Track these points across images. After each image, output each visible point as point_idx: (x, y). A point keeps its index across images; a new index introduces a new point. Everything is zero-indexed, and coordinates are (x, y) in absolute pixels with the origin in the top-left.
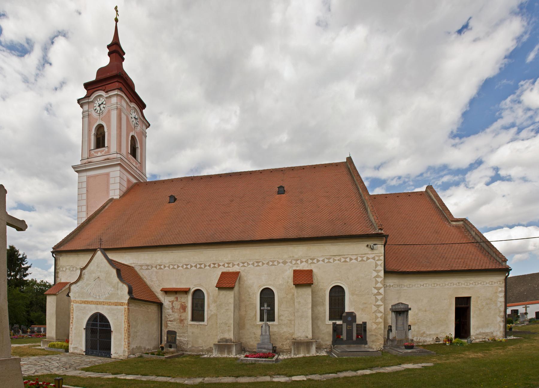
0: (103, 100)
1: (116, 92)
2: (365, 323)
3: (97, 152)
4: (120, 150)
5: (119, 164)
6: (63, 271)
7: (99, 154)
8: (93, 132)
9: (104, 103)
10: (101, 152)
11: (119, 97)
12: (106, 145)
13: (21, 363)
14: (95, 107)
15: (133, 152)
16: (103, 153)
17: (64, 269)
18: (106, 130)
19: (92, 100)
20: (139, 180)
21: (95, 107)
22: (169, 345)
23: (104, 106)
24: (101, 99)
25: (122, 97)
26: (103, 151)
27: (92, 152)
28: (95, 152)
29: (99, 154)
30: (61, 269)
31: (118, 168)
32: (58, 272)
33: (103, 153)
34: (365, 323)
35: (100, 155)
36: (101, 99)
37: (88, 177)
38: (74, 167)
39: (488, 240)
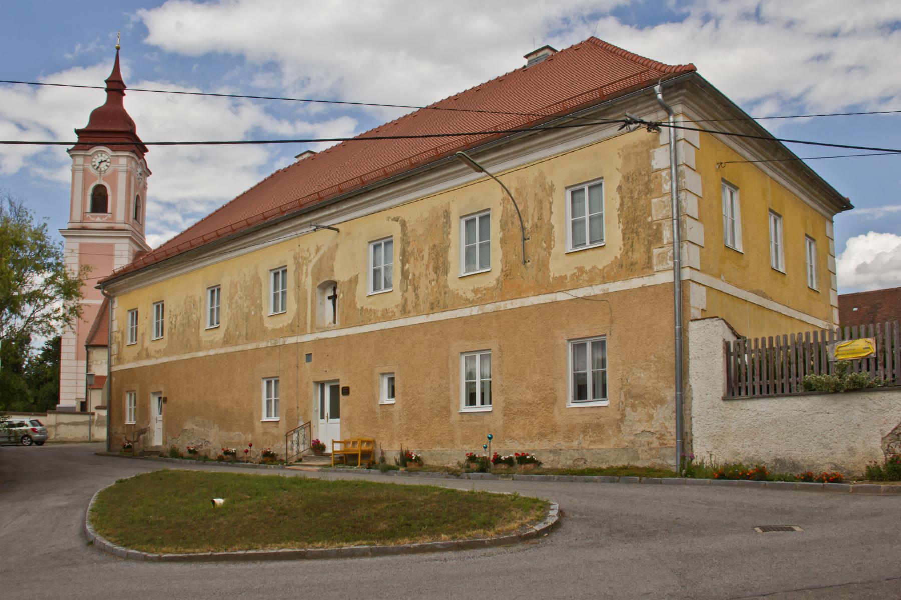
0: (107, 157)
1: (127, 154)
2: (78, 132)
3: (96, 217)
4: (128, 220)
5: (130, 238)
6: (96, 364)
7: (98, 220)
8: (90, 192)
9: (108, 161)
10: (102, 218)
11: (129, 159)
12: (109, 210)
13: (157, 441)
14: (94, 162)
15: (136, 218)
16: (105, 219)
17: (99, 363)
18: (109, 192)
19: (90, 154)
20: (143, 248)
21: (94, 162)
22: (343, 394)
23: (108, 164)
24: (103, 155)
25: (132, 158)
26: (105, 217)
27: (88, 216)
28: (92, 217)
29: (98, 220)
30: (95, 363)
31: (127, 241)
32: (90, 366)
33: (105, 219)
34: (78, 132)
35: (98, 221)
36: (103, 155)
37: (81, 245)
38: (61, 231)
39: (649, 59)
